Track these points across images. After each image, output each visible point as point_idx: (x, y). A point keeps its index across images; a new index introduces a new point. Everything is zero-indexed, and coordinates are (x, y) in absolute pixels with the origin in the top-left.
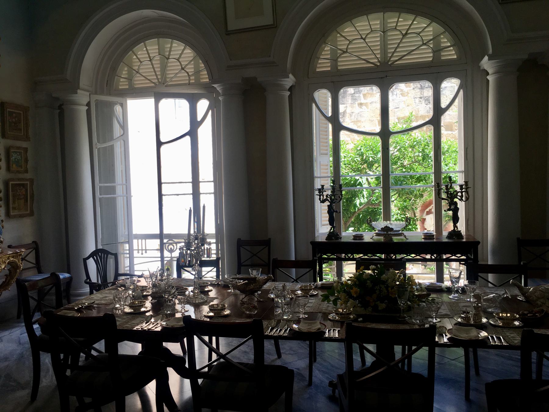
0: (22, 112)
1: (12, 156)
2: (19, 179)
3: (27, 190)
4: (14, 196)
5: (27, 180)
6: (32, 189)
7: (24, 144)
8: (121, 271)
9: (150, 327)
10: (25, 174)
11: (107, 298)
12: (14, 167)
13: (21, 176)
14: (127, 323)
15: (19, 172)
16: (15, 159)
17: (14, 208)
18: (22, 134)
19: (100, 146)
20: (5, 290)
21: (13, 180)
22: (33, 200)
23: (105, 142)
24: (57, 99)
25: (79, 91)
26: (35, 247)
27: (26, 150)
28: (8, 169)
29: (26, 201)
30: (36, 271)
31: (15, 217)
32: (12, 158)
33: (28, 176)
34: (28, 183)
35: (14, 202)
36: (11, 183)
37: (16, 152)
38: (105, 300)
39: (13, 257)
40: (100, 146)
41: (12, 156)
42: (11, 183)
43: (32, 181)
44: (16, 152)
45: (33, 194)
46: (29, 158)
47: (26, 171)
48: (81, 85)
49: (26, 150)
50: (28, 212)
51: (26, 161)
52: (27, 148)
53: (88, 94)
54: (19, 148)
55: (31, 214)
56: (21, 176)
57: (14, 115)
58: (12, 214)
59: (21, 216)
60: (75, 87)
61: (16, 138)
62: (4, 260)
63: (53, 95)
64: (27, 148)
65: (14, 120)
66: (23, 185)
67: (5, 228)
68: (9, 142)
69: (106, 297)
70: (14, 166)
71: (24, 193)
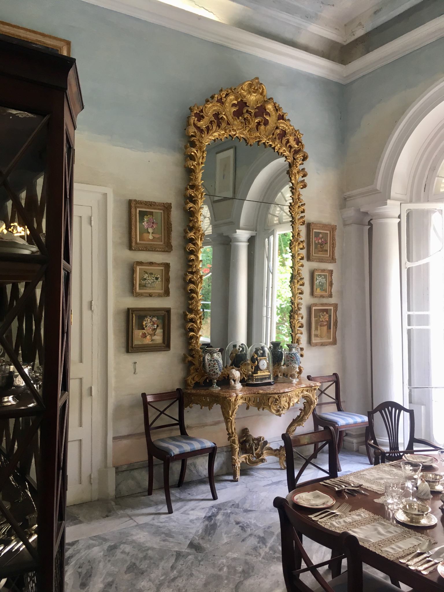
0: (328, 232)
1: (317, 280)
2: (322, 305)
3: (330, 316)
4: (317, 323)
5: (330, 305)
6: (336, 316)
7: (330, 266)
8: (416, 436)
9: (420, 568)
10: (330, 299)
11: (382, 482)
12: (318, 292)
13: (325, 301)
14: (390, 541)
15: (322, 296)
16: (320, 282)
17: (316, 336)
18: (328, 256)
19: (409, 265)
20: (299, 425)
21: (316, 305)
22: (336, 328)
23: (419, 259)
24: (366, 214)
25: (389, 201)
26: (336, 379)
27: (331, 272)
28: (312, 293)
29: (329, 328)
30: (334, 407)
31: (316, 345)
32: (317, 282)
33: (332, 301)
34: (332, 308)
35: (316, 329)
36: (314, 308)
37: (320, 275)
38: (379, 484)
39: (307, 391)
40: (409, 265)
41: (317, 280)
42: (314, 308)
43: (336, 306)
44: (320, 275)
45: (336, 320)
46: (333, 282)
47: (331, 296)
48: (393, 194)
49: (331, 272)
50: (331, 340)
51: (331, 284)
52: (332, 271)
53: (399, 203)
54: (323, 271)
55: (334, 342)
56: (325, 301)
57: (321, 236)
58: (313, 341)
59: (323, 345)
60: (384, 196)
61: (321, 260)
62: (297, 393)
63: (361, 210)
64: (332, 271)
65: (320, 241)
66: (326, 311)
67: (305, 356)
68: (315, 265)
69: (382, 479)
70: (318, 290)
71: (327, 319)
